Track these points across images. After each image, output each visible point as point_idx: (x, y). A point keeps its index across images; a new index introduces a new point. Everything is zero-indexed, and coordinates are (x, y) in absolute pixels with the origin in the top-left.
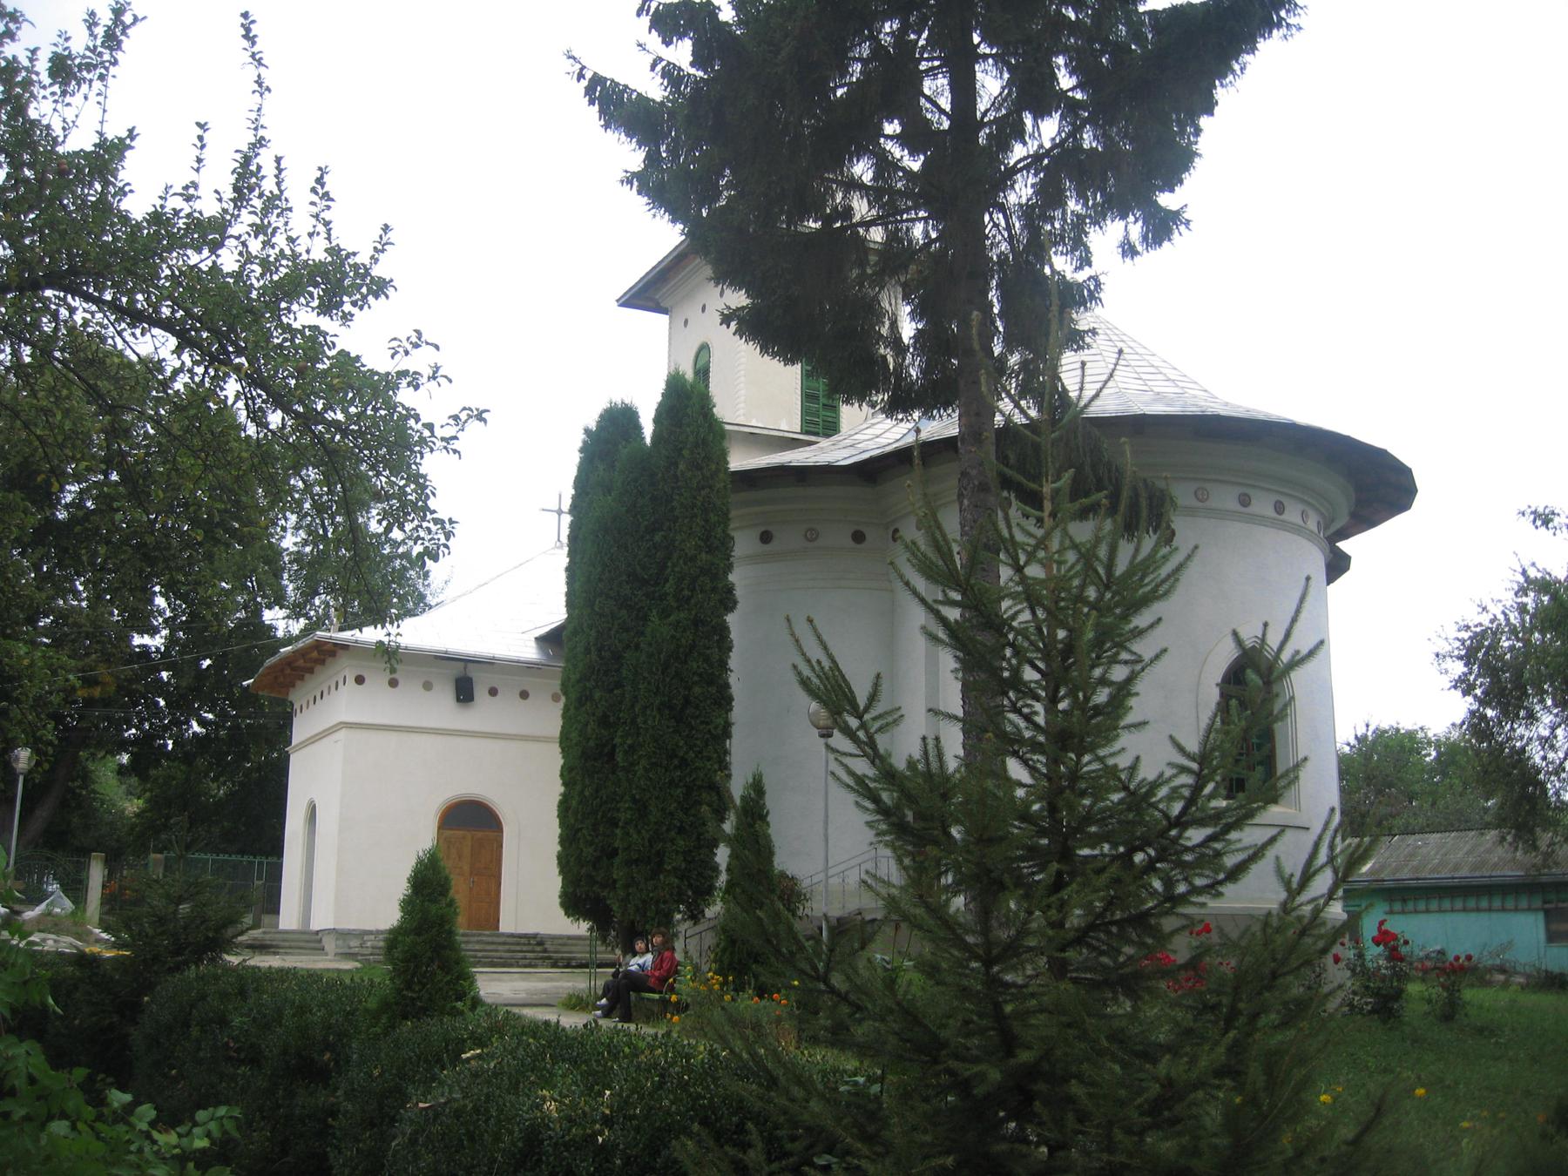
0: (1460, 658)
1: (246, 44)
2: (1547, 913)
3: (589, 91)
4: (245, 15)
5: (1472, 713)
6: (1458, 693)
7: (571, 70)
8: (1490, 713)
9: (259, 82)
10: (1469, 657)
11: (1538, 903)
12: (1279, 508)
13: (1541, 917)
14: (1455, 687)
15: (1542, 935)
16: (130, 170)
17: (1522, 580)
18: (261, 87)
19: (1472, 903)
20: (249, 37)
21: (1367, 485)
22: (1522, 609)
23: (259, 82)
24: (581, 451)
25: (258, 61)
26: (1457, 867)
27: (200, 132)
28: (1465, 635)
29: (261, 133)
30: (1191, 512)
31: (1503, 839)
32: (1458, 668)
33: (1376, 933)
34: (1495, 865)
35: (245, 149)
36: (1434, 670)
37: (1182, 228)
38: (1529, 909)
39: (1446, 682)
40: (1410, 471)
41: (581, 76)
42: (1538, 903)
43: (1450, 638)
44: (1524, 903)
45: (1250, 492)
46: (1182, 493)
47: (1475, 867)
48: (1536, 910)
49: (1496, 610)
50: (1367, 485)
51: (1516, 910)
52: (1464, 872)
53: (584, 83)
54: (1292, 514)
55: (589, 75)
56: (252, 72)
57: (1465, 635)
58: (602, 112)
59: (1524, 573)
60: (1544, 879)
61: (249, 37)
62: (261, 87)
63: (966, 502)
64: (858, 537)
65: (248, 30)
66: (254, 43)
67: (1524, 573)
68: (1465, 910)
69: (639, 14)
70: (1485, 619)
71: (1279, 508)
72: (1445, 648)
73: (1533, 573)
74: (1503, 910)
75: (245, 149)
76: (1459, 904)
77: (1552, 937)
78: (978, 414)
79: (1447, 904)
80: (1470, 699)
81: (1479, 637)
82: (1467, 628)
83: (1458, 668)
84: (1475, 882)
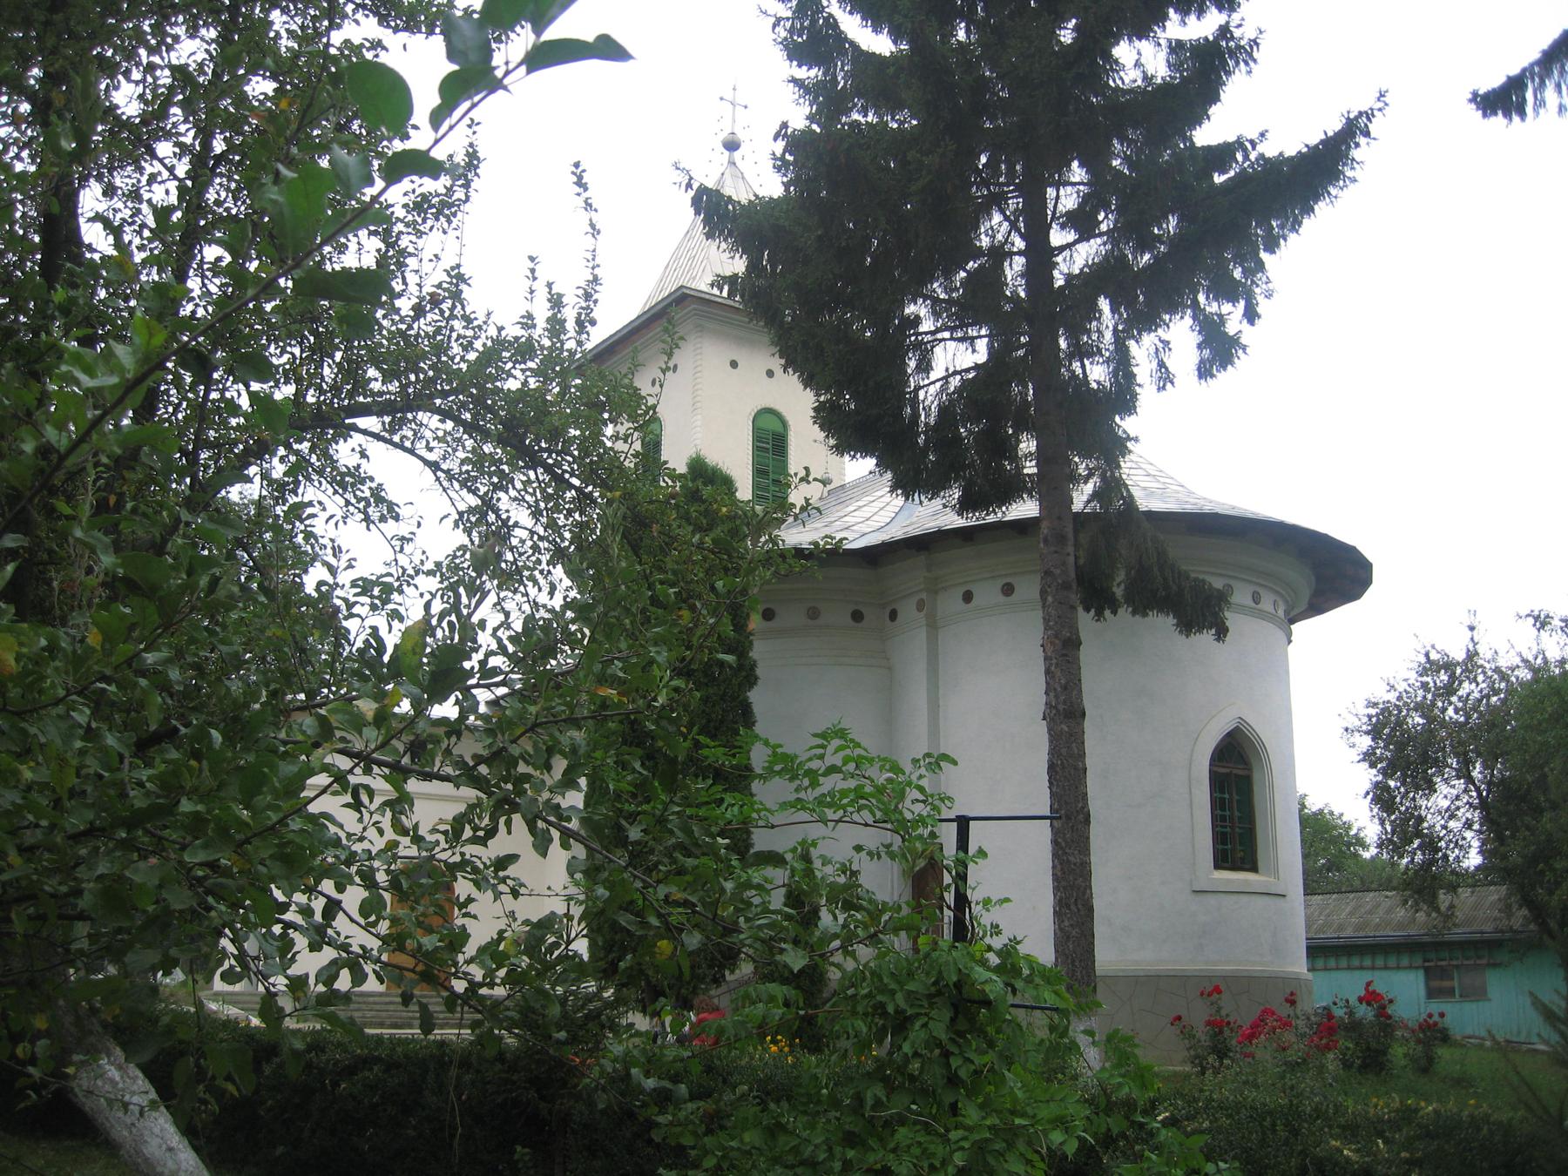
0: (1367, 733)
1: (578, 190)
2: (1427, 971)
3: (696, 202)
4: (577, 165)
5: (1376, 785)
6: (1366, 765)
7: (678, 180)
8: (1392, 783)
9: (592, 226)
10: (1375, 732)
11: (1418, 961)
12: (1256, 598)
13: (1421, 975)
14: (1364, 760)
15: (1422, 992)
16: (476, 299)
17: (1423, 660)
18: (594, 230)
19: (1356, 961)
20: (580, 183)
21: (1327, 573)
22: (1424, 686)
23: (592, 226)
24: (1145, 615)
25: (588, 205)
26: (1341, 928)
27: (531, 265)
28: (1373, 711)
29: (596, 271)
30: (1242, 610)
31: (1406, 902)
32: (1366, 742)
33: (1363, 993)
34: (1378, 926)
35: (583, 284)
36: (1343, 745)
37: (1240, 352)
38: (1410, 967)
39: (1354, 755)
40: (1371, 565)
41: (689, 186)
42: (1418, 961)
43: (1359, 714)
44: (1405, 961)
45: (1262, 591)
46: (1241, 596)
47: (1358, 928)
48: (1417, 968)
49: (1402, 687)
50: (1327, 573)
51: (1398, 968)
52: (1349, 932)
53: (691, 193)
54: (1267, 605)
55: (695, 186)
56: (584, 217)
57: (1373, 711)
58: (706, 222)
59: (1427, 655)
60: (1447, 938)
61: (580, 183)
62: (594, 230)
63: (1050, 599)
64: (857, 616)
65: (580, 178)
66: (586, 189)
67: (1427, 655)
68: (1349, 968)
69: (775, 139)
70: (1392, 697)
71: (1256, 598)
72: (1353, 722)
73: (1434, 656)
74: (1386, 968)
75: (583, 284)
76: (1344, 962)
77: (1431, 994)
78: (1059, 518)
79: (1332, 963)
80: (1374, 771)
81: (1385, 711)
82: (1375, 705)
83: (1366, 742)
84: (1360, 942)
